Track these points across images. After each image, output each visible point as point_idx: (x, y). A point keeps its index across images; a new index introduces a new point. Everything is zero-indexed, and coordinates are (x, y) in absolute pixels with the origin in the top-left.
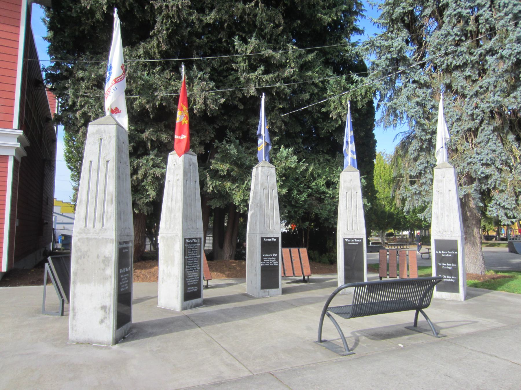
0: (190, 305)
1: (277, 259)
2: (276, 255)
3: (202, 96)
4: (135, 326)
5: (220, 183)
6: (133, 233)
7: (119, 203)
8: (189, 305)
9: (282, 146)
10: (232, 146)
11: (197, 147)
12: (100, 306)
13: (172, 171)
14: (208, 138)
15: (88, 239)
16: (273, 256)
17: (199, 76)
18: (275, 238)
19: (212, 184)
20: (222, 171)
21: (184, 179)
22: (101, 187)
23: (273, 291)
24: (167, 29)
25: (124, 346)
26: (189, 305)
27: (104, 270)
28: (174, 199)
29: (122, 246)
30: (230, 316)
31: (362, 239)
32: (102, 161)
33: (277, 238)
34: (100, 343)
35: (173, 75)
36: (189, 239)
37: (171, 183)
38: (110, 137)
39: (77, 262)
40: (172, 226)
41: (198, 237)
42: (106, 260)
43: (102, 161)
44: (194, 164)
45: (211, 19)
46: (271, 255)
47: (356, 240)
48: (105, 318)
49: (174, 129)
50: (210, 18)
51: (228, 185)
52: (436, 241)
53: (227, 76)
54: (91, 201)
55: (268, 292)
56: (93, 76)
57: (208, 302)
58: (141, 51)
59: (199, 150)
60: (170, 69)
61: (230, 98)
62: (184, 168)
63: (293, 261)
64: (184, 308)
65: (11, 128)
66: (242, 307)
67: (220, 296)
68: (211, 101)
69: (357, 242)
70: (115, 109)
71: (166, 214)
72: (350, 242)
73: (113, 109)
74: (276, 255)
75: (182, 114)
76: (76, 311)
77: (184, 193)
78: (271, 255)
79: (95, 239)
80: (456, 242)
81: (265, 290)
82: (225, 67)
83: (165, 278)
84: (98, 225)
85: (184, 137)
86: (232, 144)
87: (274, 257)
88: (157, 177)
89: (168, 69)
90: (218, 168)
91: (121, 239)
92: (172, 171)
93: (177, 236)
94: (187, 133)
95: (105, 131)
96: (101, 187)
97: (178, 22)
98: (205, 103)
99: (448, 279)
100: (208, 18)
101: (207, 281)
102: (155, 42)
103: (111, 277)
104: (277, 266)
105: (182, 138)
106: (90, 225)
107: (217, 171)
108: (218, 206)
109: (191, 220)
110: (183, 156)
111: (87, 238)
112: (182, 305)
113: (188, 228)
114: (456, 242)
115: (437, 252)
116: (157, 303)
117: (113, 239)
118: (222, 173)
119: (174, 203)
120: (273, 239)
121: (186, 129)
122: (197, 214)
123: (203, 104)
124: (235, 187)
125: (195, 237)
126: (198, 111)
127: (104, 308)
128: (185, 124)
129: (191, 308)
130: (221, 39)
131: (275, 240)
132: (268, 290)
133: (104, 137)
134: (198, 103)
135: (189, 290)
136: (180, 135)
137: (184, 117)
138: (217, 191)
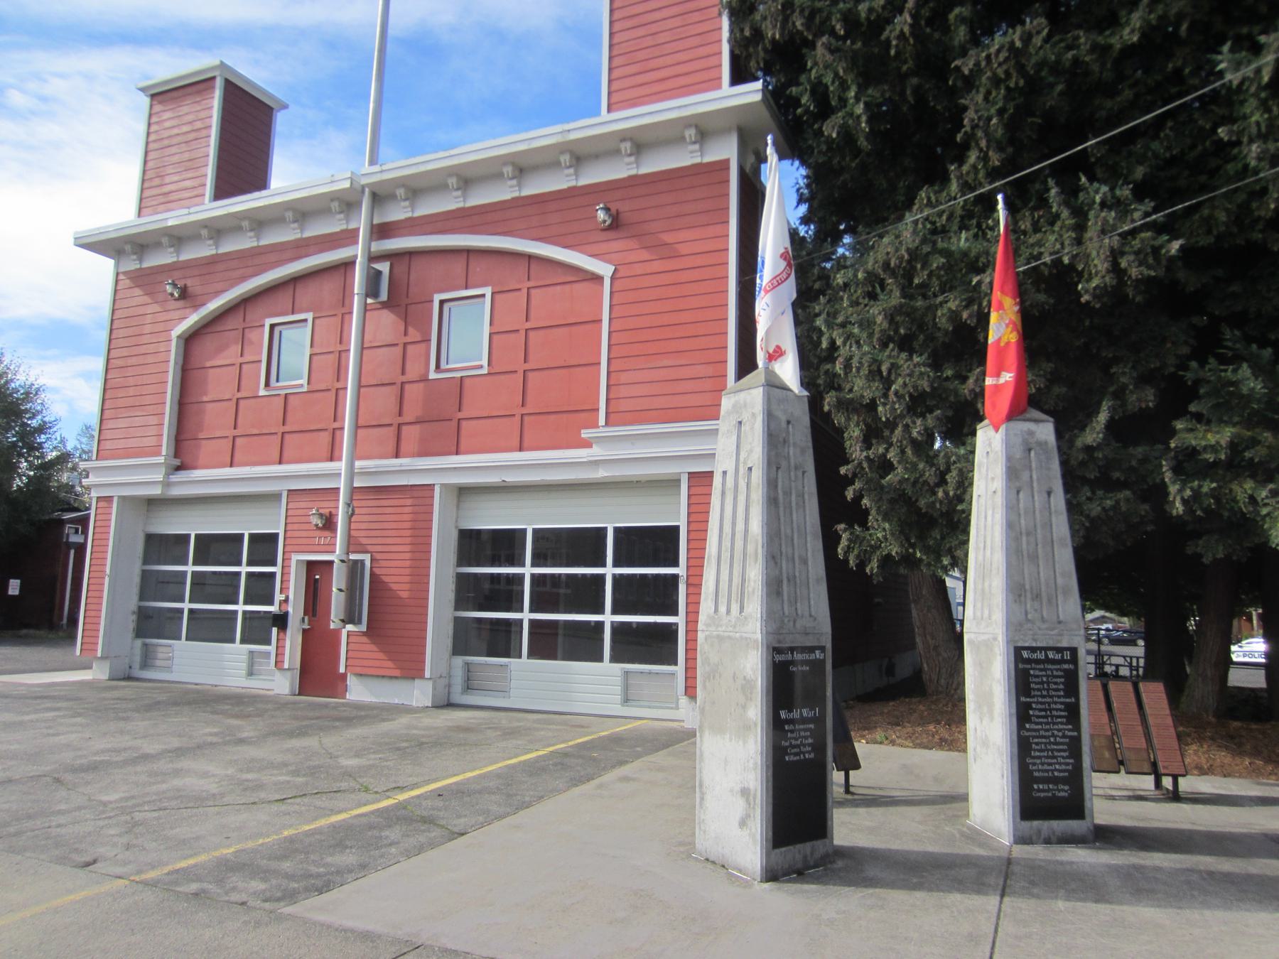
0: (1045, 833)
3: (1105, 252)
4: (841, 853)
5: (1214, 485)
6: (825, 626)
7: (773, 557)
8: (1039, 832)
9: (928, 390)
10: (1245, 371)
11: (1132, 392)
12: (738, 788)
13: (984, 470)
14: (1171, 360)
15: (720, 639)
17: (1098, 199)
19: (1180, 491)
20: (1214, 448)
21: (1008, 488)
22: (740, 526)
24: (1001, 112)
25: (779, 889)
26: (1039, 832)
27: (744, 707)
28: (988, 543)
29: (779, 658)
30: (1140, 887)
32: (742, 470)
34: (740, 871)
35: (1040, 217)
36: (1033, 649)
37: (982, 500)
38: (753, 415)
39: (704, 687)
40: (986, 612)
41: (1065, 644)
42: (747, 686)
43: (742, 470)
44: (1042, 445)
45: (1133, 31)
48: (748, 816)
49: (982, 360)
50: (1129, 34)
51: (1243, 489)
53: (1219, 168)
54: (726, 555)
56: (860, 275)
57: (1106, 836)
58: (954, 187)
59: (1139, 400)
60: (1032, 204)
61: (1235, 230)
62: (1009, 459)
64: (1021, 840)
66: (1211, 874)
67: (1245, 831)
68: (1132, 258)
70: (775, 351)
71: (975, 583)
73: (771, 351)
75: (1001, 318)
76: (704, 790)
77: (1010, 526)
79: (729, 637)
82: (1208, 143)
83: (978, 749)
84: (735, 607)
85: (1007, 377)
86: (1245, 365)
89: (1025, 205)
90: (1194, 443)
91: (779, 642)
92: (984, 470)
93: (995, 639)
94: (1014, 367)
95: (745, 405)
96: (740, 526)
97: (1022, 83)
98: (1116, 269)
100: (1127, 30)
101: (1175, 778)
102: (973, 157)
103: (756, 725)
105: (1002, 381)
106: (723, 609)
107: (1192, 453)
108: (1220, 555)
109: (1037, 597)
110: (1002, 429)
111: (718, 636)
112: (1015, 829)
113: (1028, 620)
116: (967, 815)
117: (756, 641)
118: (1210, 457)
119: (988, 552)
121: (1012, 357)
122: (1060, 581)
123: (1108, 271)
124: (1264, 494)
125: (1051, 644)
126: (1095, 296)
127: (745, 792)
128: (1008, 344)
129: (1048, 841)
130: (1178, 71)
133: (745, 417)
134: (1097, 273)
135: (1039, 790)
136: (998, 375)
137: (1007, 325)
138: (1204, 510)
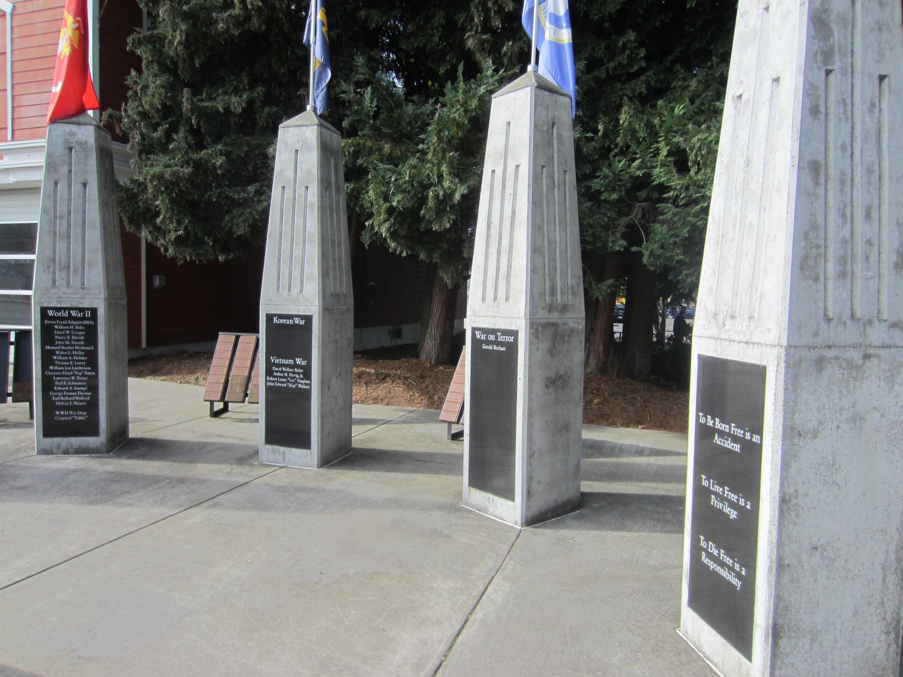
1: (307, 375)
2: (304, 363)
16: (295, 366)
18: (302, 317)
23: (294, 454)
31: (514, 334)
33: (308, 319)
41: (86, 305)
46: (291, 362)
47: (501, 338)
52: (701, 358)
55: (284, 453)
63: (223, 380)
65: (6, 141)
69: (502, 344)
72: (488, 342)
74: (304, 363)
78: (291, 362)
80: (758, 374)
81: (276, 447)
87: (300, 367)
88: (171, 183)
99: (723, 564)
104: (307, 394)
114: (758, 374)
115: (702, 421)
120: (297, 321)
125: (74, 305)
131: (302, 322)
132: (282, 449)
